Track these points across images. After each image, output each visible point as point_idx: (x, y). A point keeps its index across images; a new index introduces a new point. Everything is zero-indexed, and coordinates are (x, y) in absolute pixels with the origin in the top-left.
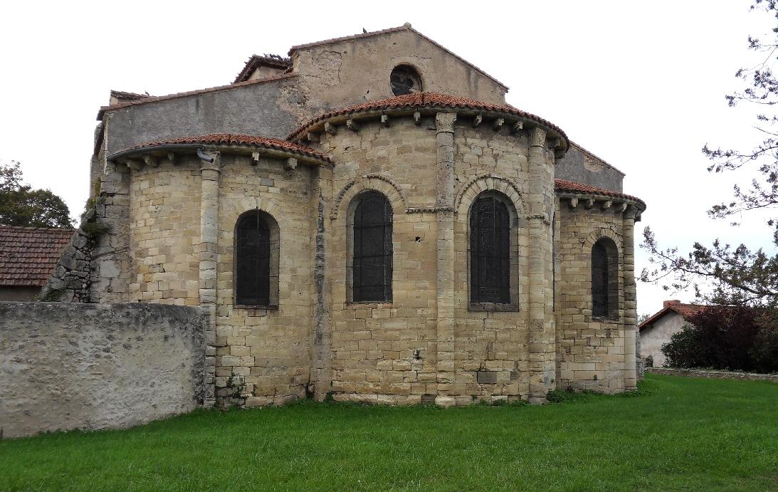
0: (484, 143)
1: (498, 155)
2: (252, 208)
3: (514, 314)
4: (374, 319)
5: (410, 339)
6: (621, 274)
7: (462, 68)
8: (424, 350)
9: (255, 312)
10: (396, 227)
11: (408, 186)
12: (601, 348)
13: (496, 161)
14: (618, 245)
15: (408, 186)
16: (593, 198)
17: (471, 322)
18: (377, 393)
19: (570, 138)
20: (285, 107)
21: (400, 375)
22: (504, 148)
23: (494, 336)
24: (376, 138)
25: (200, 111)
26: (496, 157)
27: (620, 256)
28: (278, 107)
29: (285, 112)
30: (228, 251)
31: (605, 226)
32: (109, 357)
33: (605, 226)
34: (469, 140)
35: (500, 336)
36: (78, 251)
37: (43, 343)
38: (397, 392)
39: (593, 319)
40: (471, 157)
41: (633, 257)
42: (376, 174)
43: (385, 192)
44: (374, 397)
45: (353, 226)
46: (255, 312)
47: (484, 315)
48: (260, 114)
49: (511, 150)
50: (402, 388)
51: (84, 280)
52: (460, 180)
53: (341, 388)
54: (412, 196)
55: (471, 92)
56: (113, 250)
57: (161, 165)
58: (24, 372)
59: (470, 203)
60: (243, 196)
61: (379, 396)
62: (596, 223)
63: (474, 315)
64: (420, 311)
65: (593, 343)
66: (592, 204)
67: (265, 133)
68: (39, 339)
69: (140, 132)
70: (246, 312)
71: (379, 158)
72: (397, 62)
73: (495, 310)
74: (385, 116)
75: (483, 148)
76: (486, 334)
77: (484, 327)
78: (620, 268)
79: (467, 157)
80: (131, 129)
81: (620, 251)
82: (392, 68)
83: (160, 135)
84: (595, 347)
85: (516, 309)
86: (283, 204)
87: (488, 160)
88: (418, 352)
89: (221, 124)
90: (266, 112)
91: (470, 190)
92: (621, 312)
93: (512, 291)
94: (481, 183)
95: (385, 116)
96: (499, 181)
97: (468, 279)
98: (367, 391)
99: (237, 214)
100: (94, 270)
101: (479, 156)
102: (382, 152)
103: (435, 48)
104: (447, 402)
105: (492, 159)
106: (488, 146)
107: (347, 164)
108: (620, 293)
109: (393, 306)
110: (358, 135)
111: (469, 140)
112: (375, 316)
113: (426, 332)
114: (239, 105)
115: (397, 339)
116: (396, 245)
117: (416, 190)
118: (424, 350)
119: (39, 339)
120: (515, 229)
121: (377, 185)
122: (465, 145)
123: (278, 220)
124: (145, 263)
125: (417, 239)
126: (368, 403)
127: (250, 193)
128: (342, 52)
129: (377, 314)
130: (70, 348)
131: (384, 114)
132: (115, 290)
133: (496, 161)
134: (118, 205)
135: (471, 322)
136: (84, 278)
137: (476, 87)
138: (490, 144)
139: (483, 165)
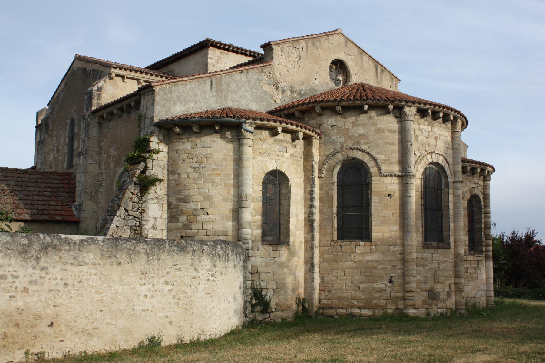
0: (429, 128)
1: (437, 137)
2: (273, 169)
3: (448, 250)
4: (357, 254)
5: (385, 268)
6: (483, 220)
7: (371, 63)
8: (395, 276)
9: (276, 247)
10: (374, 187)
11: (383, 157)
12: (474, 275)
13: (436, 141)
14: (482, 199)
15: (383, 157)
16: (470, 165)
17: (425, 256)
18: (360, 308)
19: (74, 59)
20: (266, 88)
21: (378, 294)
22: (440, 132)
23: (438, 266)
24: (357, 120)
25: (213, 89)
26: (436, 138)
27: (483, 207)
28: (261, 88)
29: (265, 91)
30: (258, 200)
31: (474, 186)
32: (214, 281)
33: (474, 186)
34: (421, 126)
35: (442, 266)
36: (134, 196)
37: (180, 270)
38: (377, 306)
39: (469, 253)
40: (422, 138)
41: (490, 208)
42: (357, 147)
43: (365, 161)
44: (357, 311)
45: (336, 184)
46: (276, 247)
47: (432, 251)
48: (250, 92)
49: (443, 134)
50: (380, 304)
51: (137, 219)
52: (416, 155)
53: (329, 305)
54: (385, 164)
55: (378, 82)
56: (157, 196)
57: (203, 132)
58: (170, 291)
59: (422, 170)
60: (267, 159)
61: (362, 310)
62: (469, 184)
63: (426, 250)
64: (391, 248)
65: (469, 271)
66: (469, 170)
67: (254, 107)
68: (178, 267)
69: (175, 104)
70: (270, 247)
71: (360, 135)
72: (333, 57)
73: (438, 248)
74: (368, 106)
75: (429, 132)
76: (434, 265)
77: (432, 260)
78: (483, 216)
79: (420, 138)
80: (170, 101)
81: (482, 204)
82: (331, 62)
83: (188, 106)
84: (471, 273)
85: (449, 247)
86: (291, 166)
87: (432, 141)
88: (391, 277)
89: (226, 99)
90: (254, 91)
91: (422, 161)
92: (484, 249)
93: (445, 234)
94: (429, 156)
95: (368, 106)
96: (438, 155)
97: (422, 225)
98: (352, 307)
99: (264, 173)
100: (144, 211)
101: (427, 138)
102: (361, 131)
103: (356, 48)
104: (414, 313)
105: (434, 140)
106: (432, 131)
107: (333, 138)
108: (483, 235)
109: (373, 244)
110: (342, 117)
111: (421, 126)
112: (357, 251)
113: (396, 263)
114: (237, 85)
115: (376, 268)
116: (374, 200)
117: (388, 160)
118: (395, 276)
119: (178, 267)
120: (447, 190)
121: (359, 155)
122: (419, 129)
123: (289, 177)
124: (189, 207)
125: (389, 195)
126: (353, 315)
127: (272, 157)
128: (300, 48)
129: (360, 249)
130: (195, 273)
131: (366, 104)
132: (158, 228)
133: (436, 141)
134: (161, 160)
135: (425, 256)
136: (137, 218)
137: (381, 78)
138: (433, 129)
139: (429, 144)
